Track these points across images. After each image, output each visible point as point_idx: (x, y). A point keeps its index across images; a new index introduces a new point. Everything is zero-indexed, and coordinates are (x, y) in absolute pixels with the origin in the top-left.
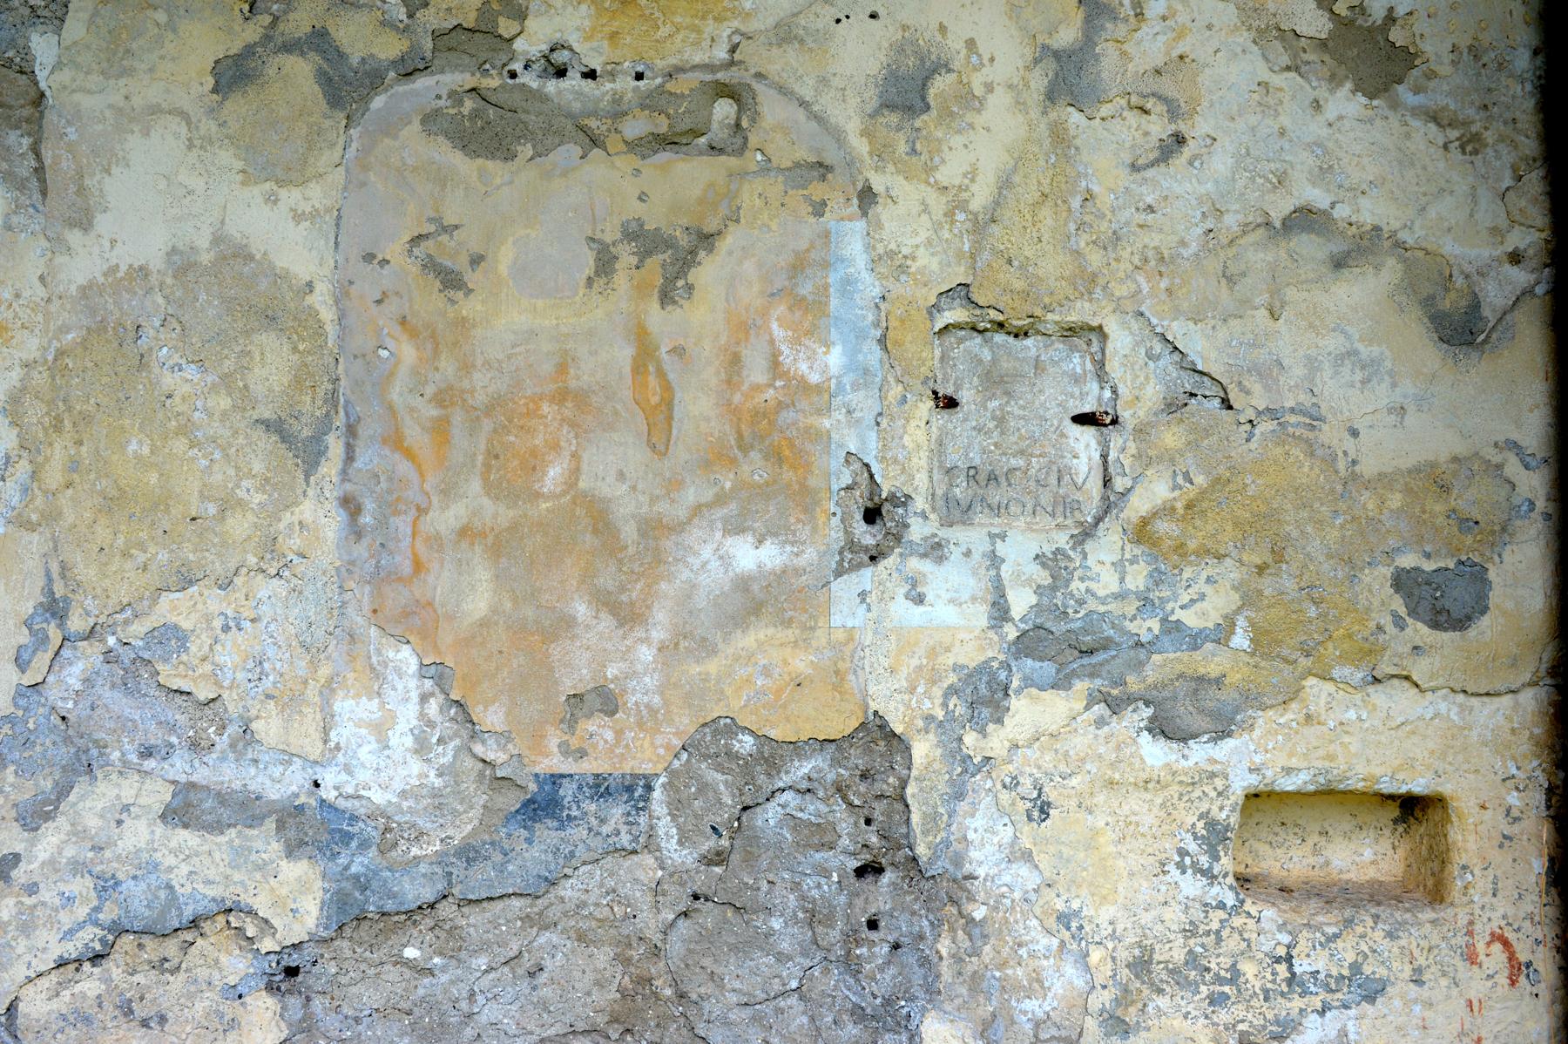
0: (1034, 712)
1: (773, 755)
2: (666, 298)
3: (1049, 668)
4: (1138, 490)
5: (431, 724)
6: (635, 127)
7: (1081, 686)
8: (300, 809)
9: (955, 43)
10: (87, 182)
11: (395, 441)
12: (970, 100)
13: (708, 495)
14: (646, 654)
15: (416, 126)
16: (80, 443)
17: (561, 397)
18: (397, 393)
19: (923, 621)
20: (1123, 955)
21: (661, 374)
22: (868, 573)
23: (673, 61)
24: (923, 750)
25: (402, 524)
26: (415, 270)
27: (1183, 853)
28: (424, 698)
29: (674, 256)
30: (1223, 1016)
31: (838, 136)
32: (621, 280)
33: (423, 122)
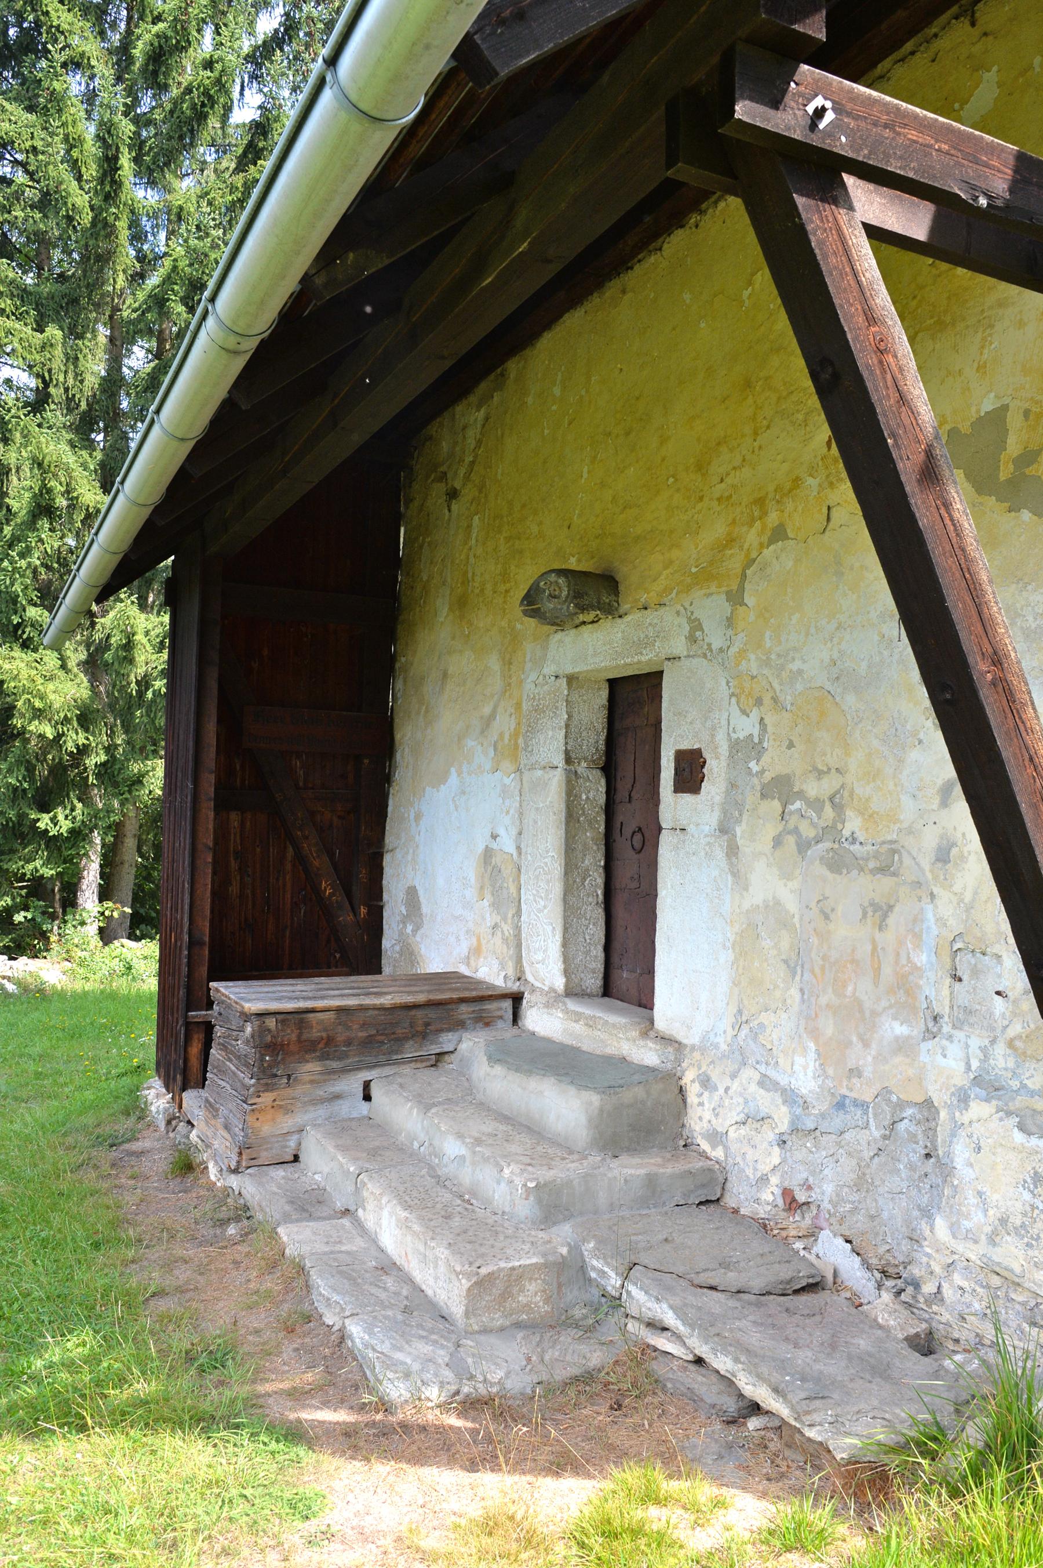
0: (979, 1109)
1: (902, 1105)
2: (880, 929)
3: (983, 1093)
4: (1011, 1027)
6: (872, 865)
7: (994, 1102)
9: (959, 835)
11: (812, 972)
12: (963, 858)
13: (887, 1004)
14: (870, 1059)
17: (853, 961)
18: (813, 955)
19: (947, 1064)
20: (999, 1215)
21: (878, 957)
22: (930, 1042)
23: (882, 839)
24: (943, 1114)
25: (813, 1000)
27: (1025, 1181)
29: (880, 912)
30: (1030, 1253)
31: (922, 870)
32: (869, 920)
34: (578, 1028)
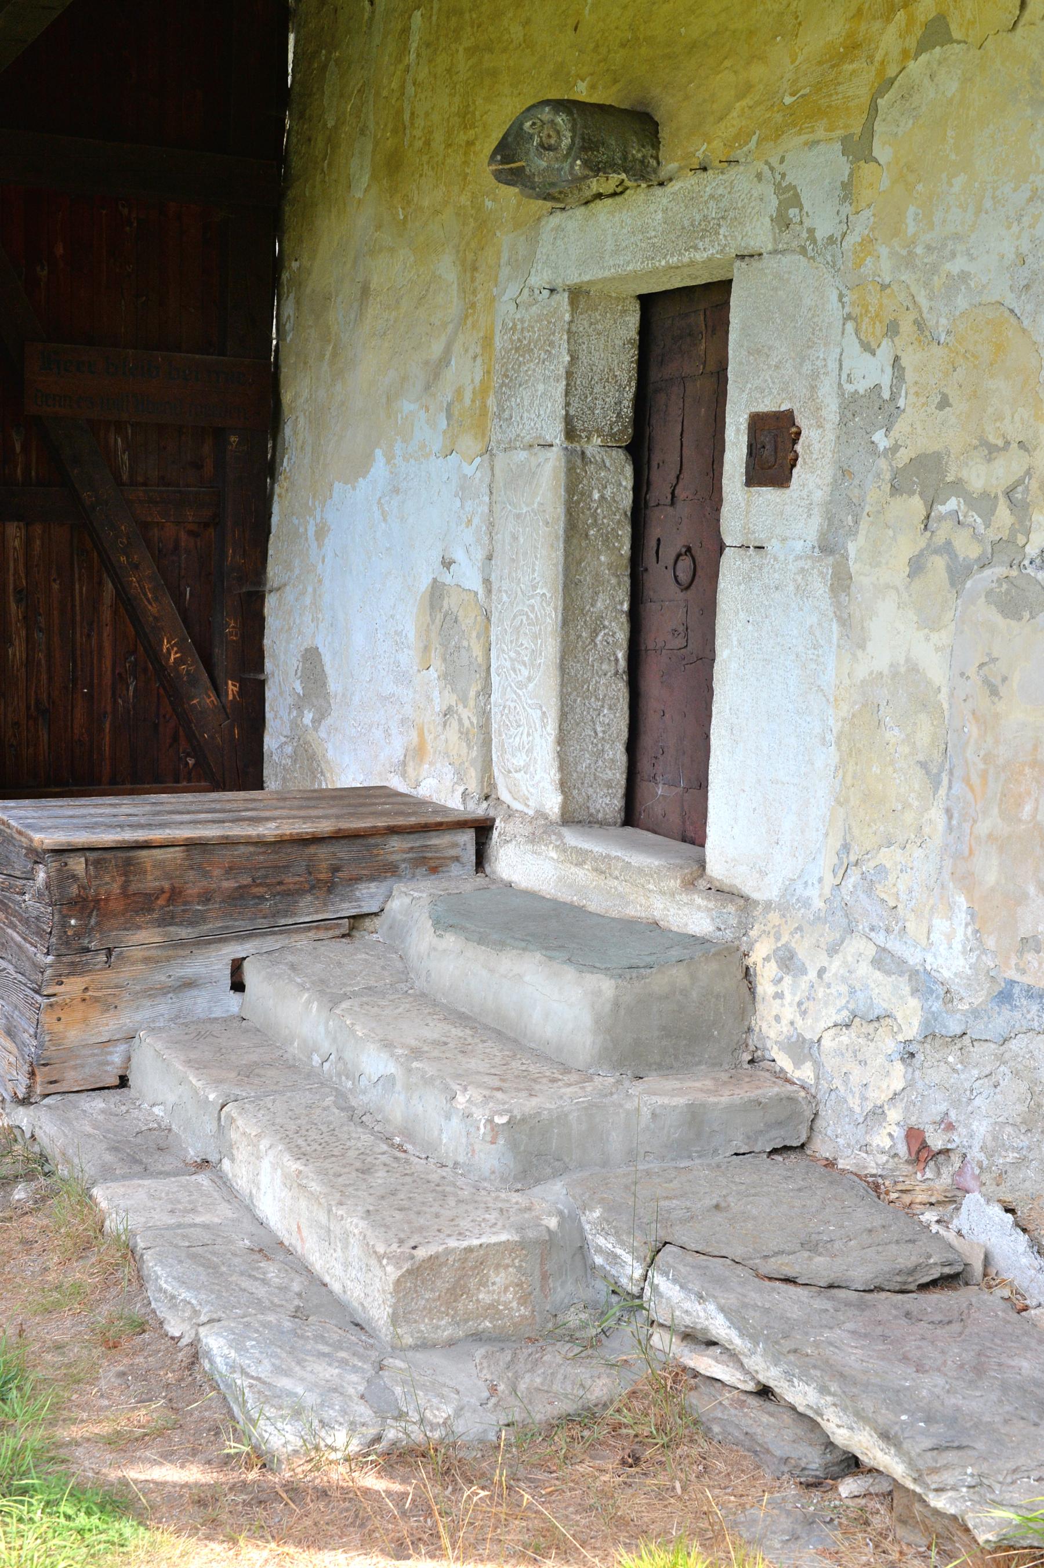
5: (968, 939)
8: (917, 971)
10: (865, 625)
15: (983, 599)
16: (857, 764)
25: (966, 826)
26: (980, 683)
28: (967, 925)
33: (986, 597)
34: (582, 875)
